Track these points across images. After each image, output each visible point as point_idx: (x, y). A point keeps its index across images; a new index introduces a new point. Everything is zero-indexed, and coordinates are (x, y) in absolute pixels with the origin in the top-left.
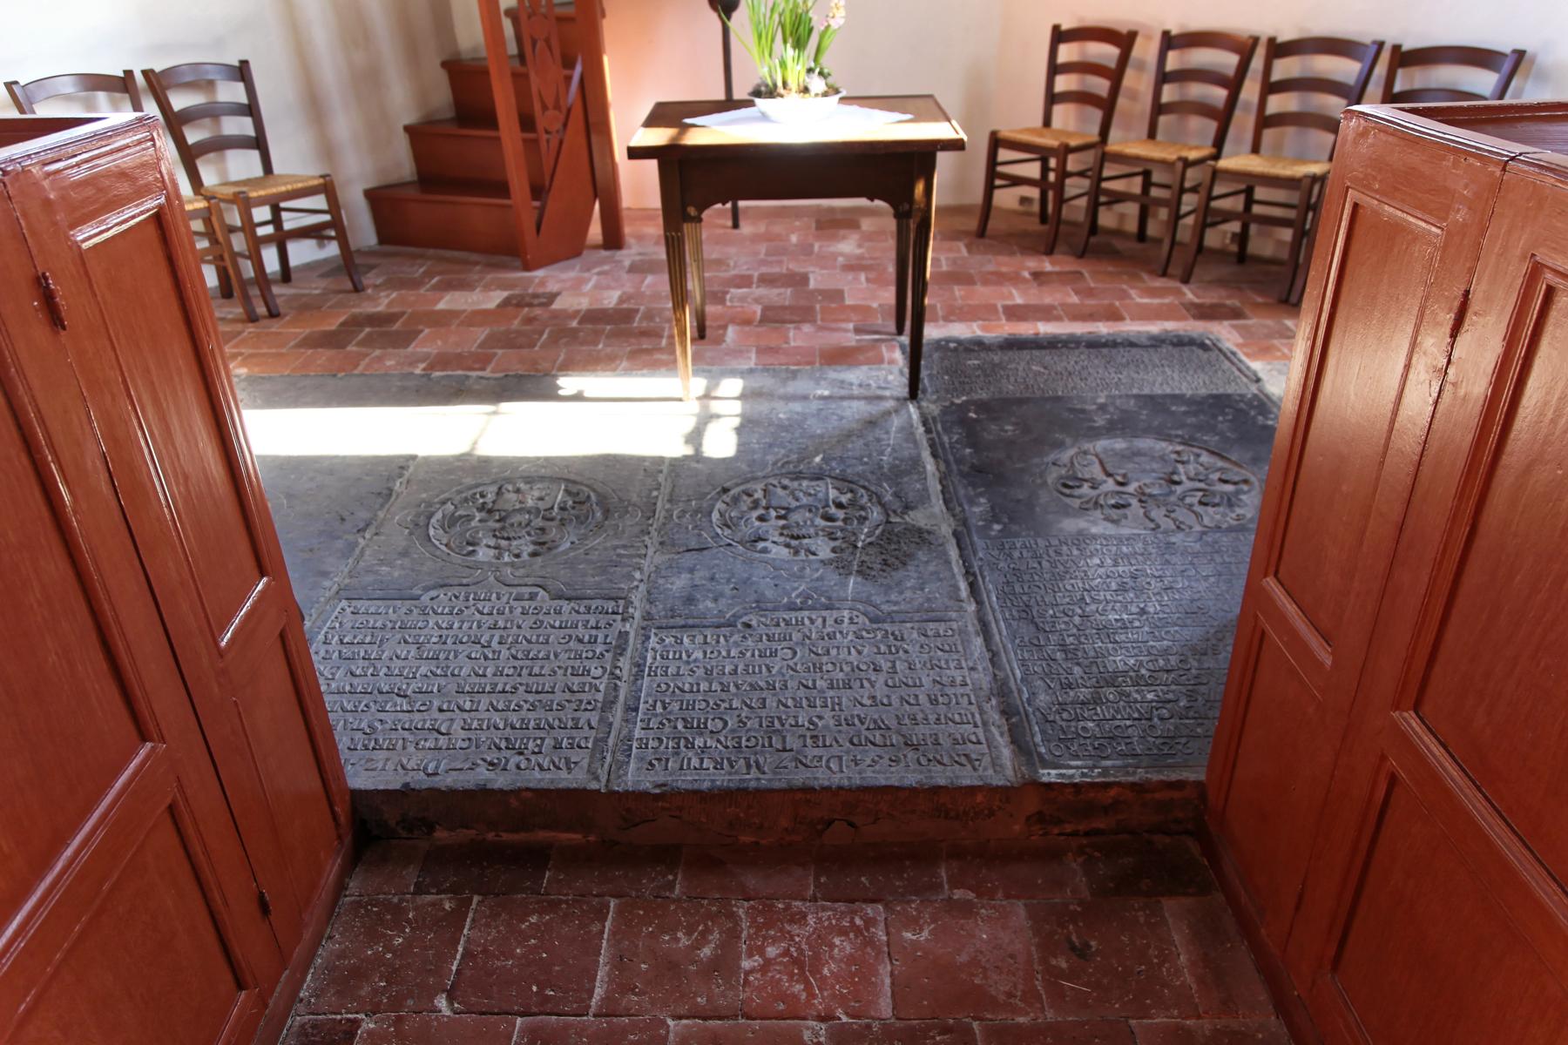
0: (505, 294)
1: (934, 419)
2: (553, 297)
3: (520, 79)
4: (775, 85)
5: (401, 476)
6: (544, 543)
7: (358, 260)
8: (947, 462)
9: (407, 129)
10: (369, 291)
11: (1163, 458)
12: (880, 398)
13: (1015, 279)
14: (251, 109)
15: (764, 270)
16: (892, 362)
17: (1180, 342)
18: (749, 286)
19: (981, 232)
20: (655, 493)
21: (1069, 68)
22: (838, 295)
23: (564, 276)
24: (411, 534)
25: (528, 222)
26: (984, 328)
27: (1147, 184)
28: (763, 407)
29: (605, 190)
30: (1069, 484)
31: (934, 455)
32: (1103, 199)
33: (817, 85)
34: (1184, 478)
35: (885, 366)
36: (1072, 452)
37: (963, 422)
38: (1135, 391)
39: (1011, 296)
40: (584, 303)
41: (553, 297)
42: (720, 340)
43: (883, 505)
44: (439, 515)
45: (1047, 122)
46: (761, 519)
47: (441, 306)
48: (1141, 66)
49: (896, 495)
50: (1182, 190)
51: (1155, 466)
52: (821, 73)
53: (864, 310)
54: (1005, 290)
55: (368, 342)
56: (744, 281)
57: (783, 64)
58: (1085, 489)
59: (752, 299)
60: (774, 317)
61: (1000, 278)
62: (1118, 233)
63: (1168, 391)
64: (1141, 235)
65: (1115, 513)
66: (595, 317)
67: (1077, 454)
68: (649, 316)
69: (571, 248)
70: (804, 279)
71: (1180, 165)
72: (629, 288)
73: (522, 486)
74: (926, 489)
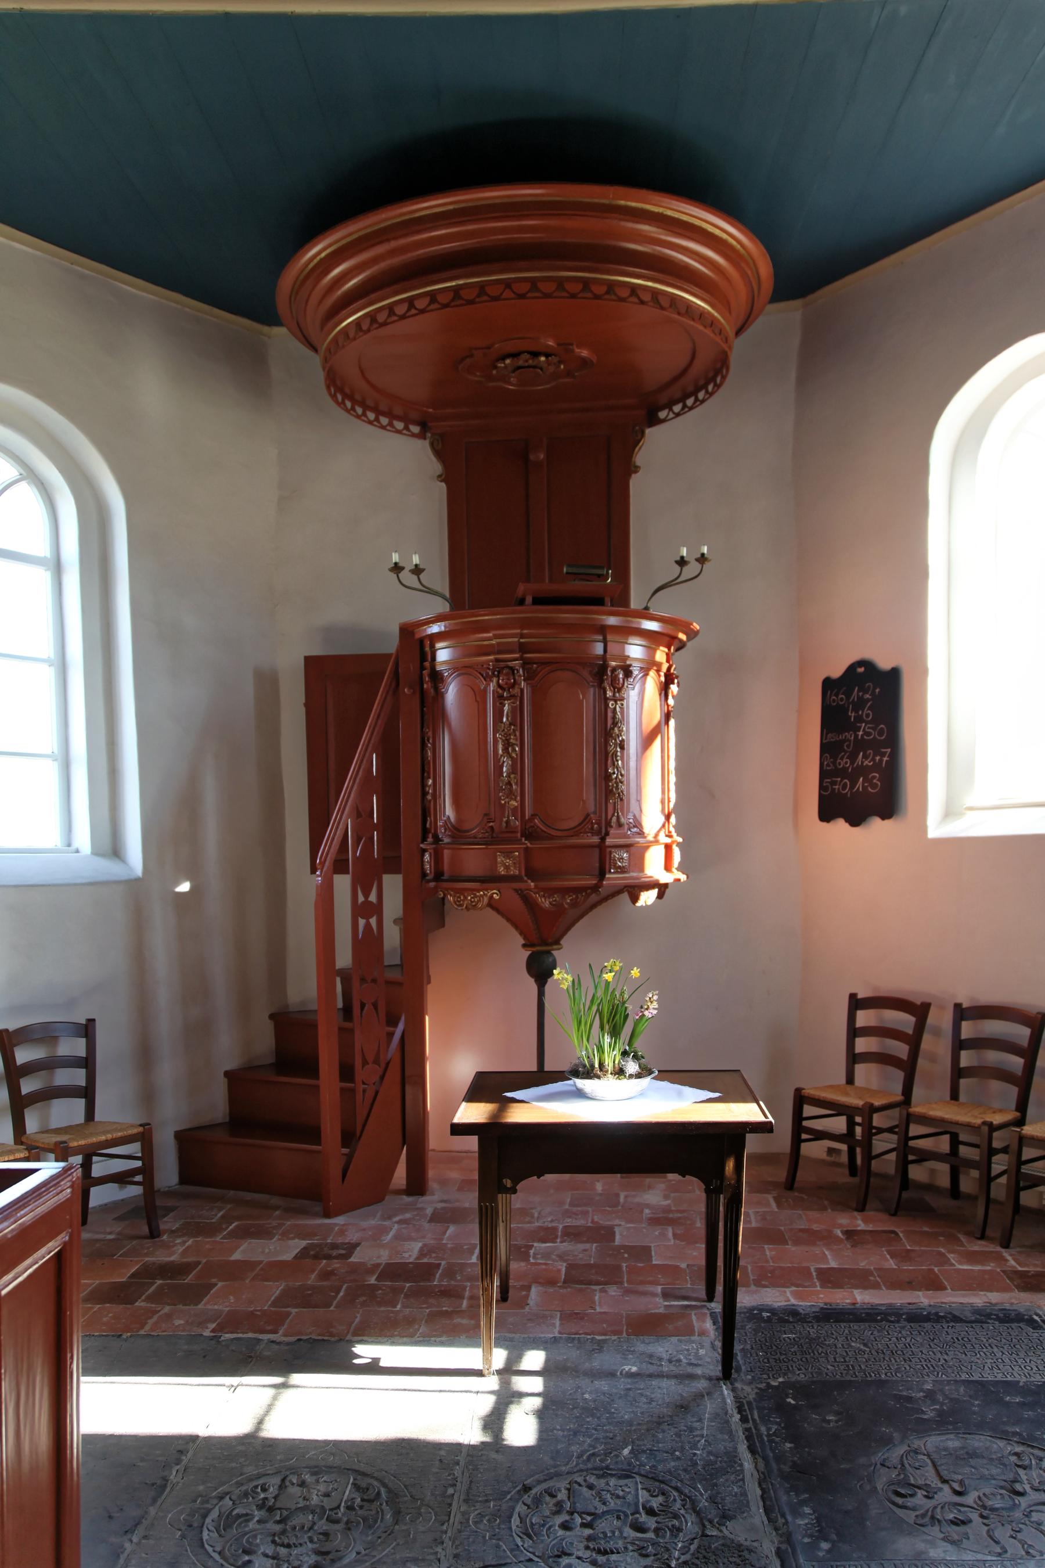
0: (304, 1243)
1: (749, 1403)
2: (352, 1247)
3: (345, 1035)
4: (592, 1066)
5: (178, 1462)
6: (327, 1553)
7: (159, 1202)
8: (765, 1458)
9: (227, 1074)
10: (165, 1237)
11: (1001, 1462)
12: (692, 1377)
13: (826, 1238)
14: (88, 1063)
15: (569, 1222)
16: (703, 1333)
17: (1008, 1318)
18: (553, 1241)
19: (790, 1184)
20: (451, 1491)
21: (867, 1031)
22: (643, 1252)
23: (365, 1224)
24: (183, 1536)
25: (335, 1168)
26: (797, 1295)
27: (955, 1142)
28: (568, 1384)
29: (412, 1132)
30: (902, 1490)
31: (752, 1450)
32: (911, 1158)
33: (632, 1067)
34: (1027, 1487)
35: (695, 1338)
36: (901, 1450)
37: (781, 1408)
38: (964, 1376)
39: (824, 1258)
40: (383, 1256)
41: (352, 1247)
42: (523, 1303)
43: (698, 1513)
44: (214, 1514)
45: (850, 1080)
46: (565, 1526)
47: (237, 1256)
48: (937, 1032)
49: (712, 1500)
50: (992, 1152)
51: (994, 1471)
52: (636, 1057)
53: (672, 1271)
54: (817, 1250)
55: (157, 1298)
56: (548, 1234)
57: (601, 1049)
58: (919, 1499)
59: (554, 1256)
60: (579, 1277)
61: (811, 1237)
62: (929, 1188)
63: (1000, 1377)
64: (955, 1191)
65: (954, 1531)
66: (394, 1272)
67: (908, 1453)
68: (450, 1272)
69: (375, 1193)
70: (608, 1234)
71: (985, 1129)
72: (430, 1241)
73: (308, 1478)
74: (744, 1494)
